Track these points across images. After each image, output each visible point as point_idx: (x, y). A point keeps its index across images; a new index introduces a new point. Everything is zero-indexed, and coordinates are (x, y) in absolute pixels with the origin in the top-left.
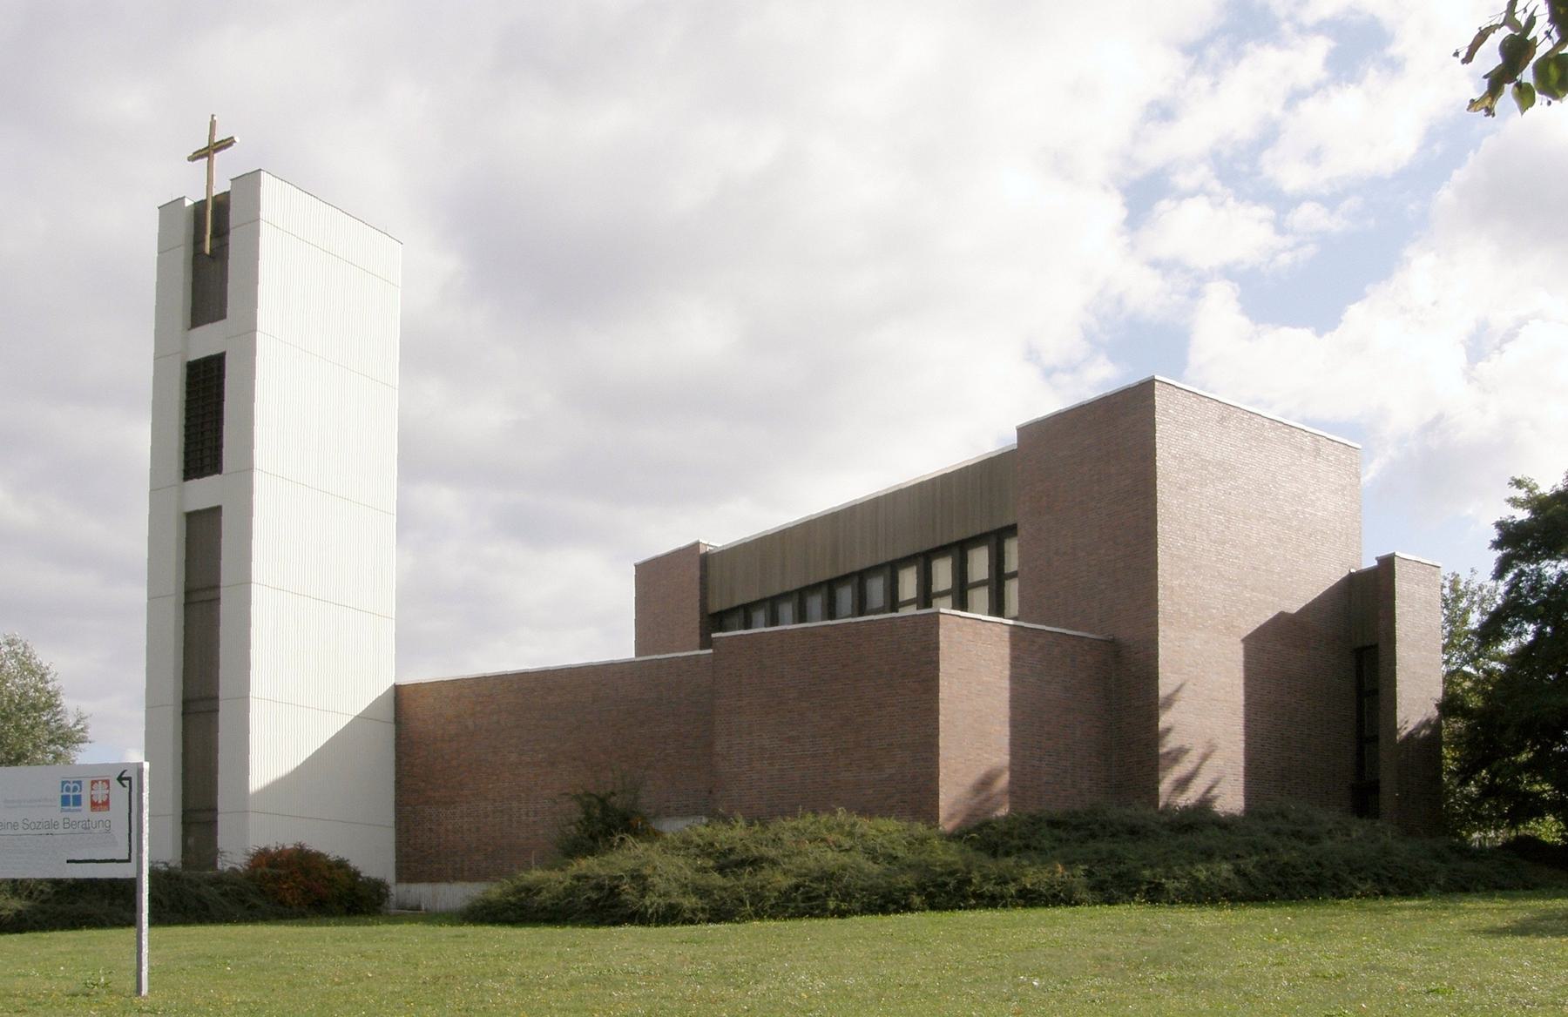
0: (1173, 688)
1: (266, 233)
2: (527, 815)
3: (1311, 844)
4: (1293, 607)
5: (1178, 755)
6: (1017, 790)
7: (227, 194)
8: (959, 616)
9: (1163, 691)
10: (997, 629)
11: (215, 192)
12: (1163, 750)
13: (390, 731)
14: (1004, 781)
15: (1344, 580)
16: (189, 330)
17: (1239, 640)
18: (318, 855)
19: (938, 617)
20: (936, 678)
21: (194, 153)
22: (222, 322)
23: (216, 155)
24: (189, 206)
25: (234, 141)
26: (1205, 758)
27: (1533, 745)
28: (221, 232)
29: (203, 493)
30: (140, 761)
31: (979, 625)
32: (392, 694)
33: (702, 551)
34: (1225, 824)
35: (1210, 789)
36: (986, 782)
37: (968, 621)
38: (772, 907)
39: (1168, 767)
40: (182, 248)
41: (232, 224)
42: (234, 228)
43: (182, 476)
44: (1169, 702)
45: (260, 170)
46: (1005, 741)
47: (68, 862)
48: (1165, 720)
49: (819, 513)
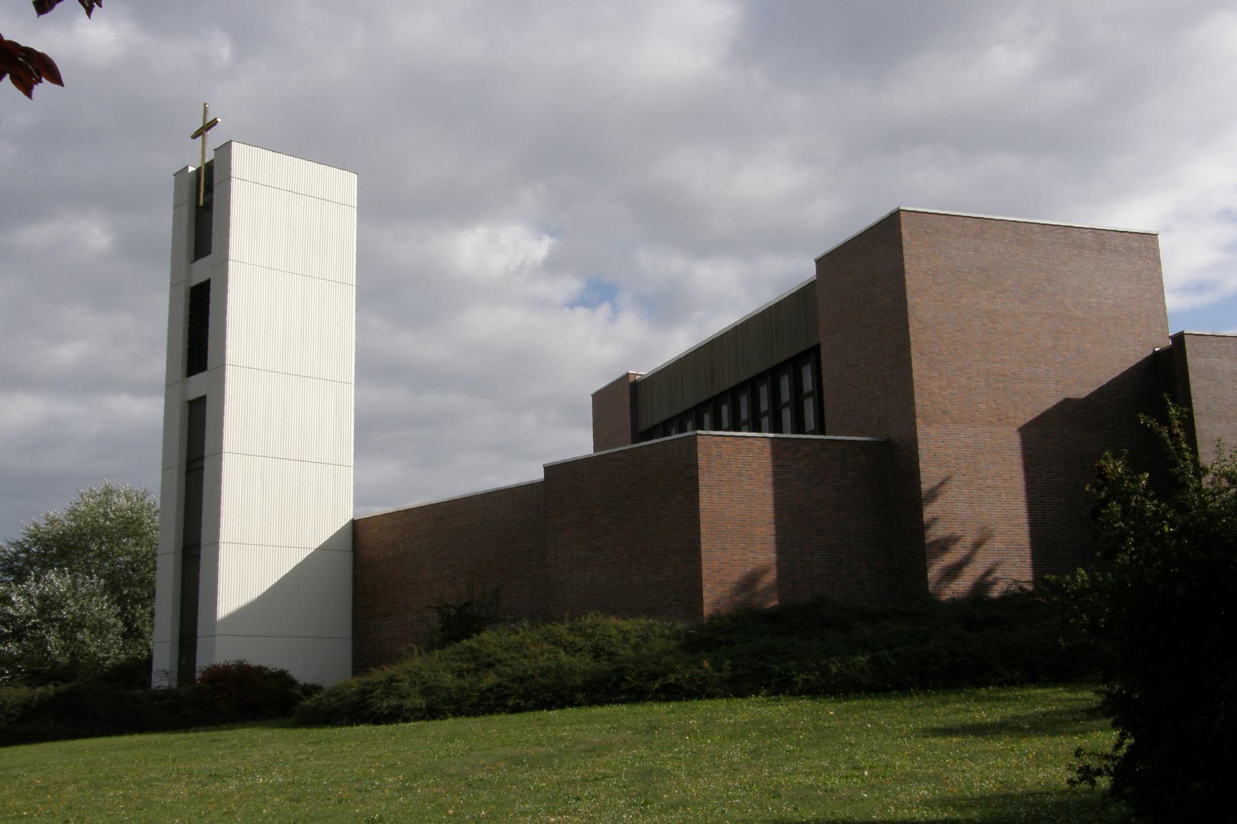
0: (936, 482)
1: (236, 186)
3: (543, 656)
4: (1081, 391)
5: (945, 545)
6: (780, 585)
8: (722, 436)
9: (925, 486)
10: (757, 442)
11: (207, 160)
12: (927, 541)
13: (348, 558)
14: (771, 578)
15: (1147, 359)
16: (192, 262)
17: (1015, 429)
18: (260, 670)
19: (696, 439)
20: (696, 490)
21: (195, 133)
24: (192, 172)
25: (217, 122)
26: (977, 545)
28: (209, 189)
29: (197, 385)
31: (741, 441)
32: (350, 529)
33: (631, 379)
34: (1016, 601)
35: (988, 573)
36: (750, 581)
37: (727, 439)
38: (472, 705)
39: (935, 556)
44: (933, 494)
45: (231, 141)
46: (771, 540)
48: (929, 512)
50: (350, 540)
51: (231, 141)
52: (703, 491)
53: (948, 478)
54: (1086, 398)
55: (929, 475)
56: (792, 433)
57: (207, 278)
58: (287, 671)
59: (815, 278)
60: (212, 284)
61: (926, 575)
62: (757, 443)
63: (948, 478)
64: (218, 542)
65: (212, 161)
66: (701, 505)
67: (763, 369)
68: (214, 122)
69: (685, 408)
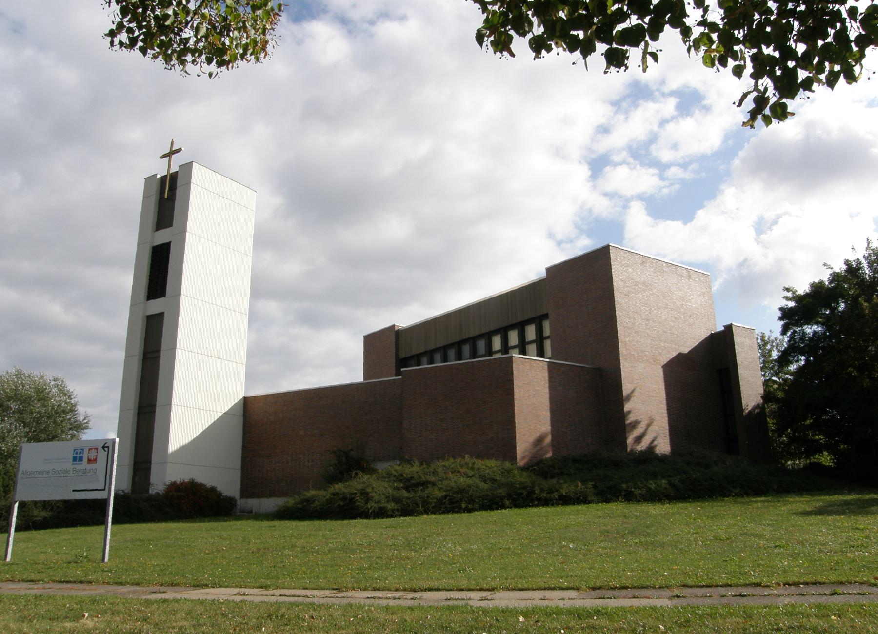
4: (686, 350)
5: (635, 424)
11: (171, 171)
12: (627, 422)
13: (241, 419)
14: (548, 439)
16: (155, 232)
18: (201, 485)
21: (163, 155)
22: (170, 228)
23: (173, 156)
26: (649, 425)
28: (173, 188)
29: (156, 306)
31: (533, 362)
32: (243, 402)
33: (396, 329)
35: (653, 441)
36: (540, 440)
37: (527, 360)
38: (433, 507)
43: (146, 298)
44: (629, 398)
45: (193, 162)
48: (627, 407)
50: (242, 408)
51: (193, 162)
52: (516, 390)
53: (634, 389)
54: (688, 352)
55: (626, 389)
56: (428, 365)
57: (170, 241)
58: (216, 487)
59: (545, 277)
60: (172, 244)
61: (626, 442)
62: (541, 364)
63: (634, 389)
64: (171, 404)
65: (176, 173)
66: (515, 397)
67: (500, 327)
68: (179, 150)
69: (453, 342)
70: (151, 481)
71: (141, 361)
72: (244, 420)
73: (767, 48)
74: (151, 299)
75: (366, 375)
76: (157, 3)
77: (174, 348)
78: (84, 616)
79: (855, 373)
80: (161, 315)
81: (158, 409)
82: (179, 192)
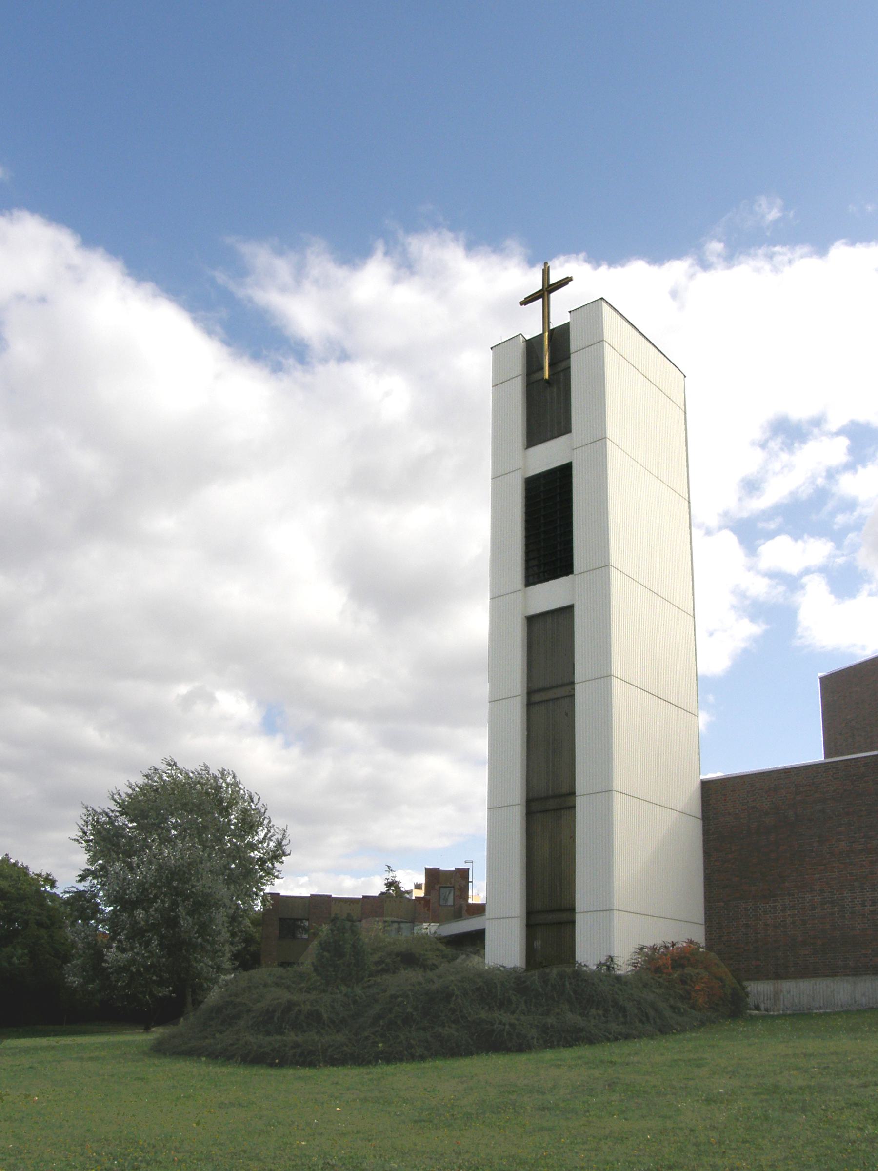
2: (863, 905)
3: (466, 911)
7: (567, 326)
11: (555, 323)
16: (525, 449)
21: (525, 299)
22: (569, 434)
23: (552, 295)
27: (107, 930)
30: (416, 890)
40: (520, 378)
41: (573, 347)
42: (573, 353)
43: (524, 583)
47: (287, 825)
49: (759, 771)
70: (576, 960)
71: (525, 706)
72: (704, 826)
73: (57, 881)
74: (534, 583)
75: (830, 747)
76: (51, 891)
77: (605, 676)
78: (168, 987)
79: (43, 883)
80: (567, 611)
81: (580, 803)
82: (577, 364)
